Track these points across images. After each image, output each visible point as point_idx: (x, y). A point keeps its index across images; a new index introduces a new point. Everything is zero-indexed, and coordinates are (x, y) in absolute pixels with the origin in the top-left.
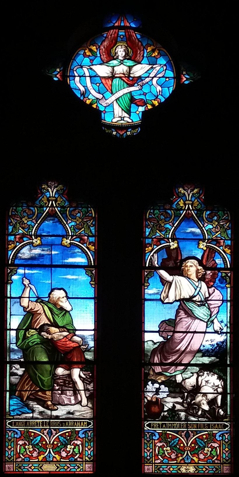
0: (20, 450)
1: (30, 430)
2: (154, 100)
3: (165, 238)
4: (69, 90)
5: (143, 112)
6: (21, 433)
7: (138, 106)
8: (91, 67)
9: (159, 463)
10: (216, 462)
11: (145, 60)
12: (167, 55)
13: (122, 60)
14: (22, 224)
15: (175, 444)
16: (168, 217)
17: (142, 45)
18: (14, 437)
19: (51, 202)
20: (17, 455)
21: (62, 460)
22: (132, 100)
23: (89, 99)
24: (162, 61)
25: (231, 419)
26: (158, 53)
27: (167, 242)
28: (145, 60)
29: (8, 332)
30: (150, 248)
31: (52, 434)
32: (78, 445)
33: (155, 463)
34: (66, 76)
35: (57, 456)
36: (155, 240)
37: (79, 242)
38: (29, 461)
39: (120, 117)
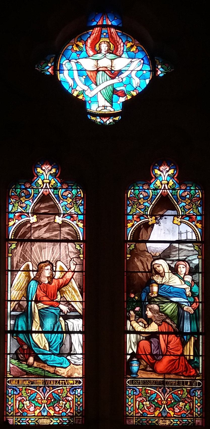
0: (139, 406)
1: (147, 388)
2: (133, 91)
3: (144, 214)
4: (59, 84)
5: (123, 102)
6: (19, 390)
7: (119, 96)
9: (140, 416)
10: (69, 414)
11: (125, 55)
12: (143, 51)
13: (105, 54)
14: (139, 205)
16: (28, 196)
17: (122, 41)
18: (14, 394)
21: (55, 414)
22: (114, 92)
23: (77, 90)
24: (140, 55)
25: (202, 377)
26: (136, 49)
27: (146, 218)
28: (125, 55)
30: (131, 223)
31: (166, 391)
32: (69, 401)
33: (135, 416)
34: (57, 69)
35: (170, 412)
36: (135, 216)
37: (189, 221)
38: (27, 416)
39: (103, 106)
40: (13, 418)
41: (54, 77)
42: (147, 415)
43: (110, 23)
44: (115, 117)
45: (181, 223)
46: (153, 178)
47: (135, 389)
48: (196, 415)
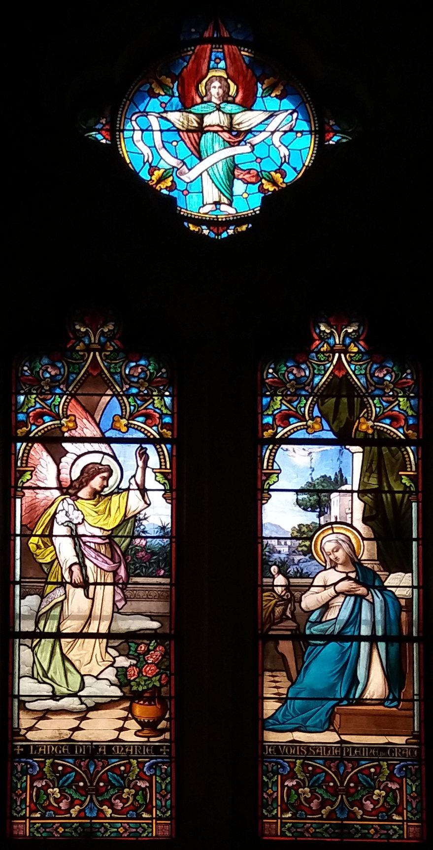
0: (288, 796)
2: (276, 172)
8: (164, 115)
9: (289, 818)
15: (70, 781)
19: (337, 355)
20: (284, 806)
29: (415, 584)
33: (281, 818)
34: (115, 131)
35: (105, 807)
37: (390, 425)
40: (25, 823)
41: (113, 149)
42: (306, 815)
43: (226, 35)
44: (240, 225)
45: (128, 428)
46: (316, 340)
47: (280, 764)
48: (156, 815)
